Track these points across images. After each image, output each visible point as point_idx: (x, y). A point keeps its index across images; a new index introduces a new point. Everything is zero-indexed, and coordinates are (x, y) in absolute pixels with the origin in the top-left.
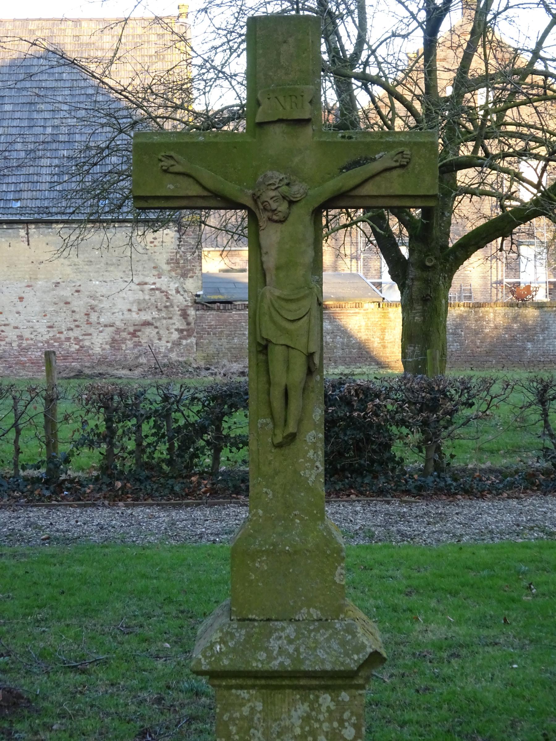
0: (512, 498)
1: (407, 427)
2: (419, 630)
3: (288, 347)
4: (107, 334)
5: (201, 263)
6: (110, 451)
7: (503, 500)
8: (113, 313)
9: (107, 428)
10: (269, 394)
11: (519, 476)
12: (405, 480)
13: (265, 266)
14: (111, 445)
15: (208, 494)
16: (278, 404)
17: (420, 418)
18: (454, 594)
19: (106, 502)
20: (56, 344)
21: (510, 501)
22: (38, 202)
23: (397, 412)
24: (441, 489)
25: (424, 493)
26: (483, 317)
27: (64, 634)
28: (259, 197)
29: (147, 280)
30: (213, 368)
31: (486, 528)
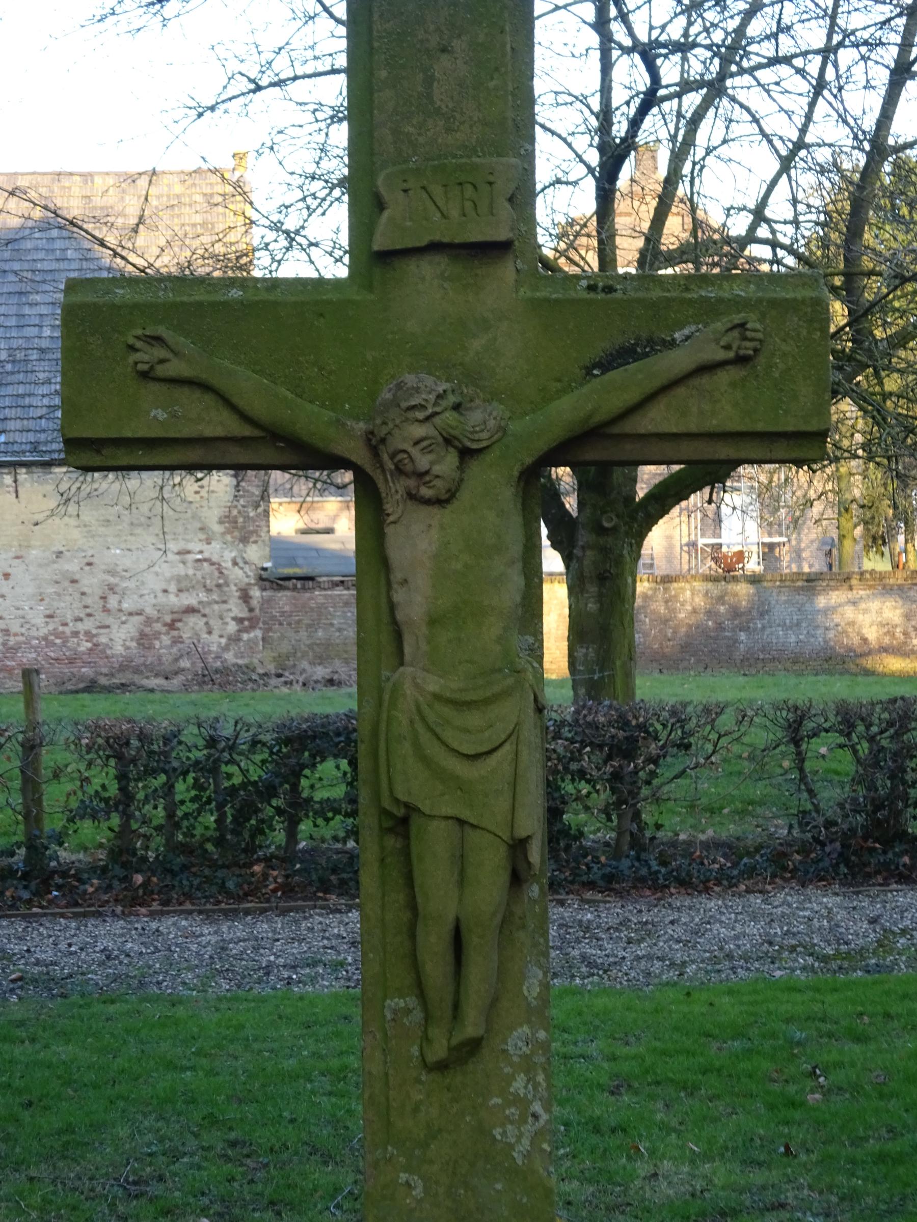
0: (753, 892)
1: (588, 782)
2: (643, 1174)
3: (461, 822)
4: (132, 626)
5: (268, 521)
6: (125, 826)
7: (740, 896)
8: (141, 596)
9: (120, 789)
10: (413, 936)
11: (762, 856)
13: (400, 616)
14: (127, 817)
15: (279, 894)
16: (436, 969)
17: (609, 769)
18: (691, 1090)
19: (119, 909)
20: (58, 641)
21: (751, 897)
22: (31, 435)
23: (572, 759)
24: (643, 880)
26: (675, 596)
27: (24, 1199)
28: (383, 441)
29: (190, 546)
30: (287, 674)
31: (721, 949)
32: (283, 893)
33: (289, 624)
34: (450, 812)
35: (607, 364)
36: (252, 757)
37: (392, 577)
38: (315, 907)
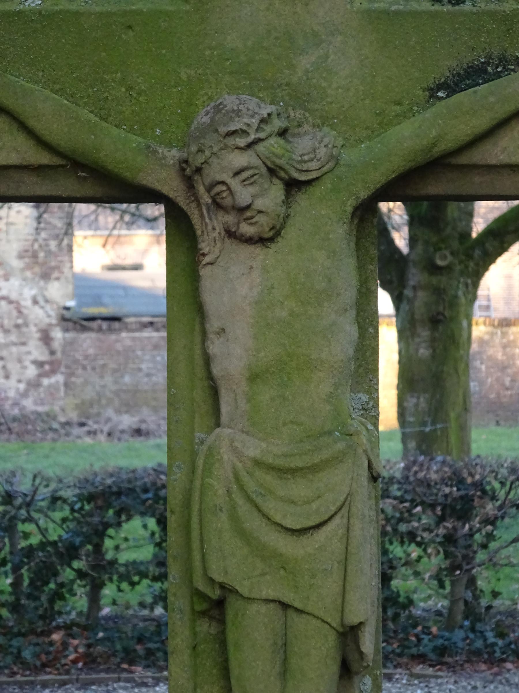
1: (419, 544)
3: (285, 606)
5: (71, 256)
12: (417, 636)
13: (216, 371)
15: (80, 665)
17: (441, 531)
23: (401, 520)
24: (478, 653)
25: (450, 660)
28: (198, 170)
30: (90, 422)
32: (85, 664)
33: (94, 369)
34: (271, 593)
35: (453, 85)
36: (50, 513)
37: (208, 326)
38: (119, 680)
